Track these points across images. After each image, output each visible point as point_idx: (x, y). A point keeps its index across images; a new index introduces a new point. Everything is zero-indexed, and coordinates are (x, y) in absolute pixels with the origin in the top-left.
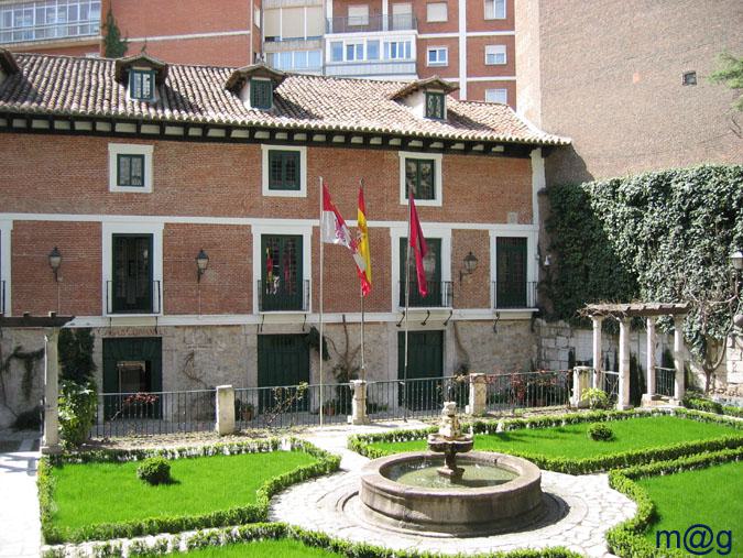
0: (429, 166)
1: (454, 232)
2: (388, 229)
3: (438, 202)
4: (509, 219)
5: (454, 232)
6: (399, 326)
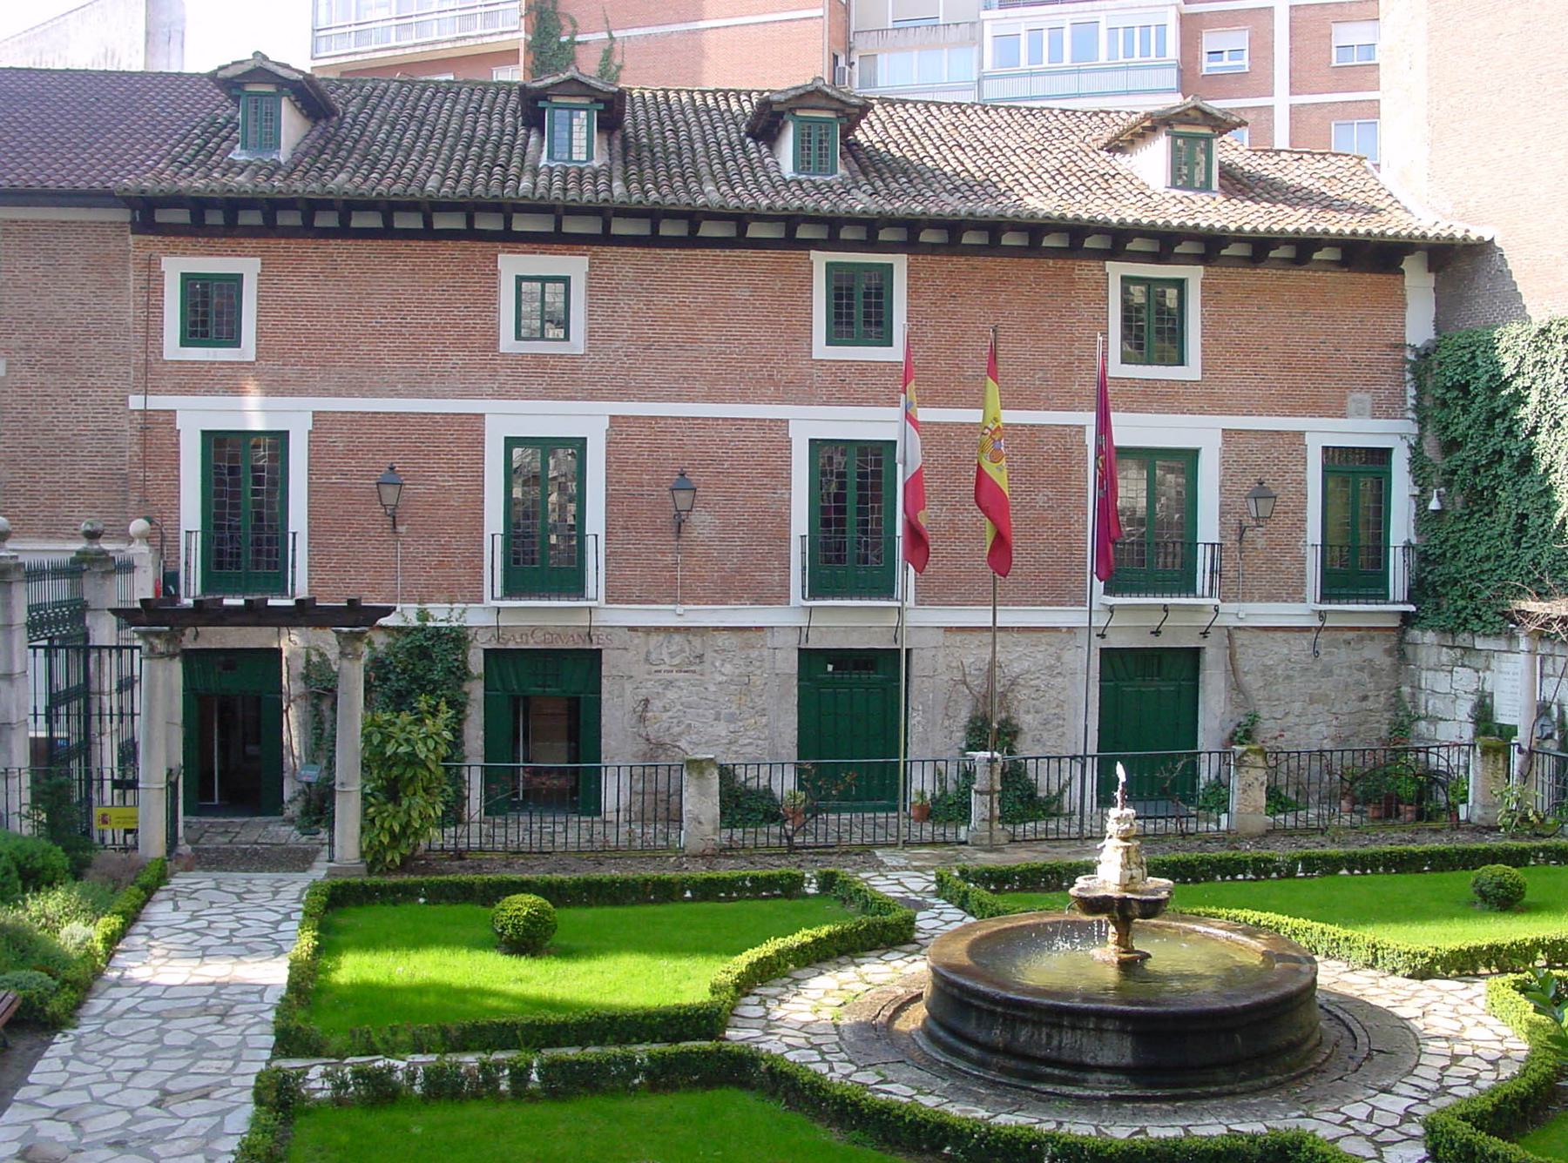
3: (1192, 370)
4: (1351, 407)
6: (1102, 636)
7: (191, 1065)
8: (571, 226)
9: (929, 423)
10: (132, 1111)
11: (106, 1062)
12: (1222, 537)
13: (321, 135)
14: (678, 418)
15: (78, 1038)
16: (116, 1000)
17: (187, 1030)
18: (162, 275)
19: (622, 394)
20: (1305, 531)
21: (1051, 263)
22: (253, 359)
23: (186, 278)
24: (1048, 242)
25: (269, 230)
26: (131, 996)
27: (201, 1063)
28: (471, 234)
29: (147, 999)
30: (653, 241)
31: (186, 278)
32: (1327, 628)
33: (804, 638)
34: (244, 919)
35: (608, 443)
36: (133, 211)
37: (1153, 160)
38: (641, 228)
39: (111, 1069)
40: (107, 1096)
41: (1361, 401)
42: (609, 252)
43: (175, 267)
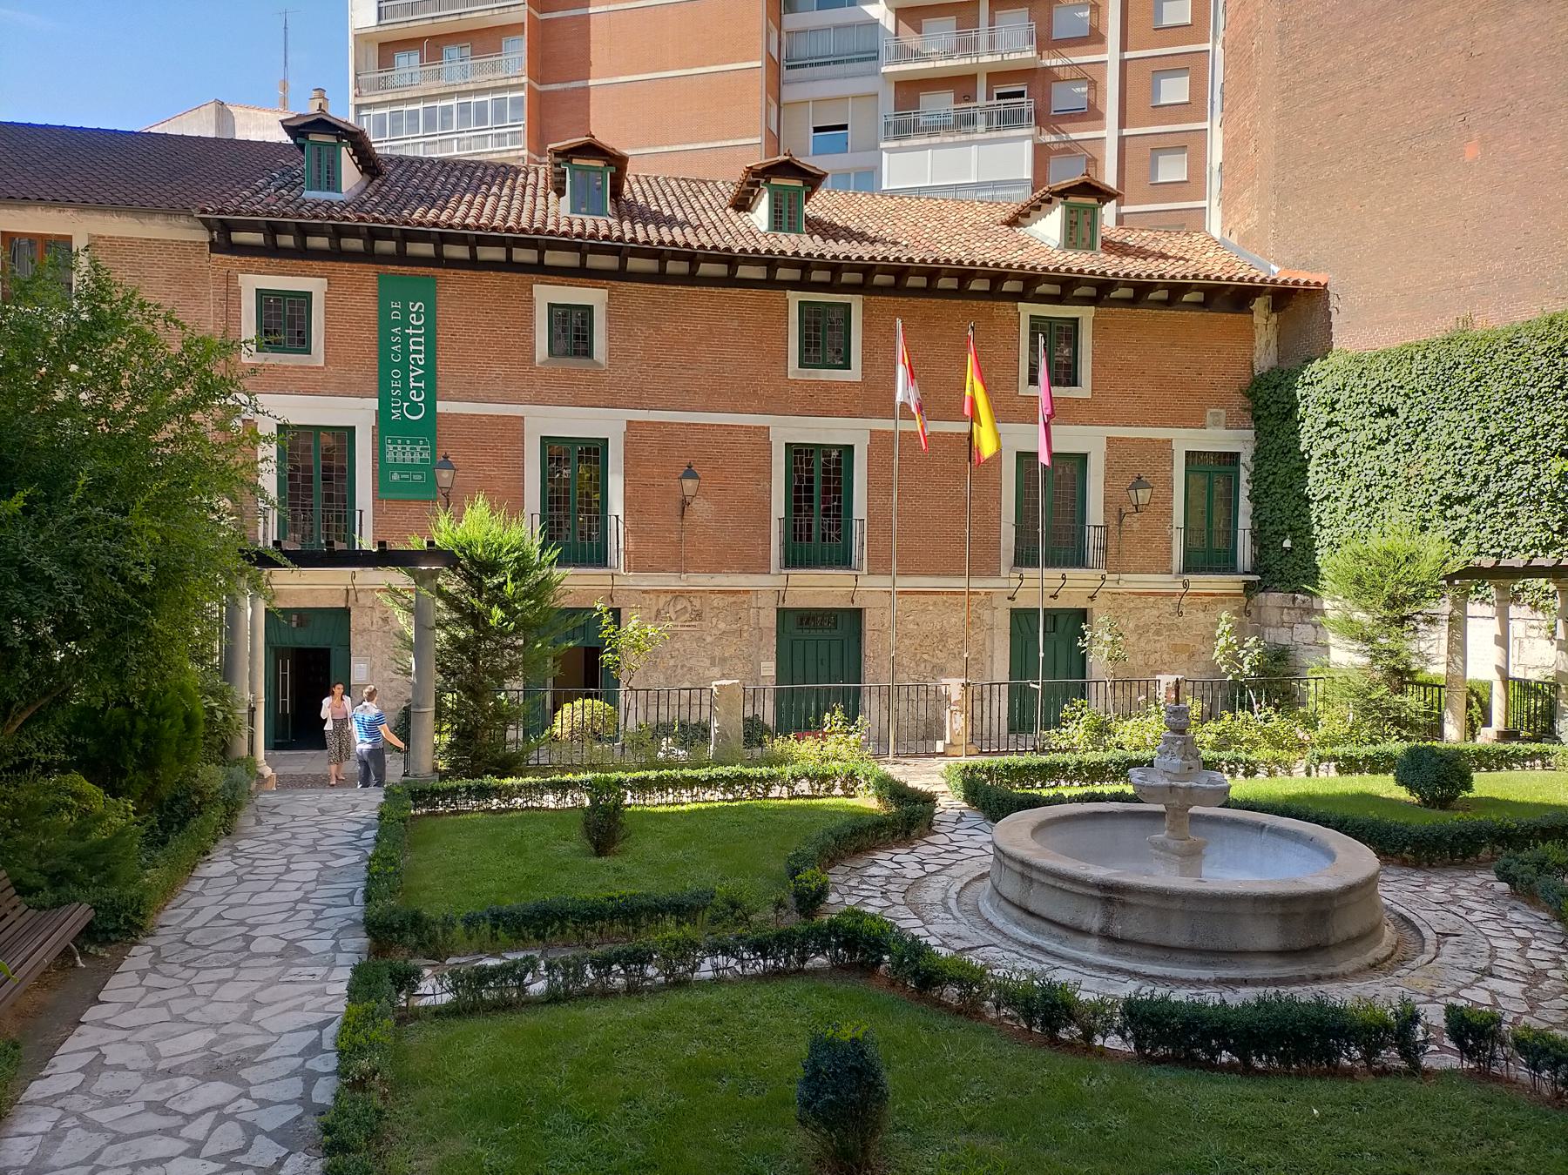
1: (1110, 441)
3: (1083, 391)
4: (1209, 419)
6: (1012, 598)
7: (283, 973)
8: (595, 261)
9: (879, 431)
10: (216, 1026)
11: (188, 973)
12: (1105, 522)
13: (377, 192)
14: (682, 424)
15: (157, 950)
16: (197, 911)
17: (276, 936)
18: (239, 289)
21: (975, 303)
22: (322, 365)
23: (260, 293)
24: (975, 285)
25: (336, 254)
26: (216, 904)
27: (295, 970)
28: (509, 266)
29: (231, 906)
30: (660, 277)
31: (260, 293)
32: (1189, 595)
33: (781, 599)
34: (327, 829)
35: (626, 443)
36: (211, 231)
37: (1049, 227)
38: (650, 265)
39: (195, 980)
40: (189, 1012)
41: (1218, 414)
42: (625, 286)
43: (253, 282)
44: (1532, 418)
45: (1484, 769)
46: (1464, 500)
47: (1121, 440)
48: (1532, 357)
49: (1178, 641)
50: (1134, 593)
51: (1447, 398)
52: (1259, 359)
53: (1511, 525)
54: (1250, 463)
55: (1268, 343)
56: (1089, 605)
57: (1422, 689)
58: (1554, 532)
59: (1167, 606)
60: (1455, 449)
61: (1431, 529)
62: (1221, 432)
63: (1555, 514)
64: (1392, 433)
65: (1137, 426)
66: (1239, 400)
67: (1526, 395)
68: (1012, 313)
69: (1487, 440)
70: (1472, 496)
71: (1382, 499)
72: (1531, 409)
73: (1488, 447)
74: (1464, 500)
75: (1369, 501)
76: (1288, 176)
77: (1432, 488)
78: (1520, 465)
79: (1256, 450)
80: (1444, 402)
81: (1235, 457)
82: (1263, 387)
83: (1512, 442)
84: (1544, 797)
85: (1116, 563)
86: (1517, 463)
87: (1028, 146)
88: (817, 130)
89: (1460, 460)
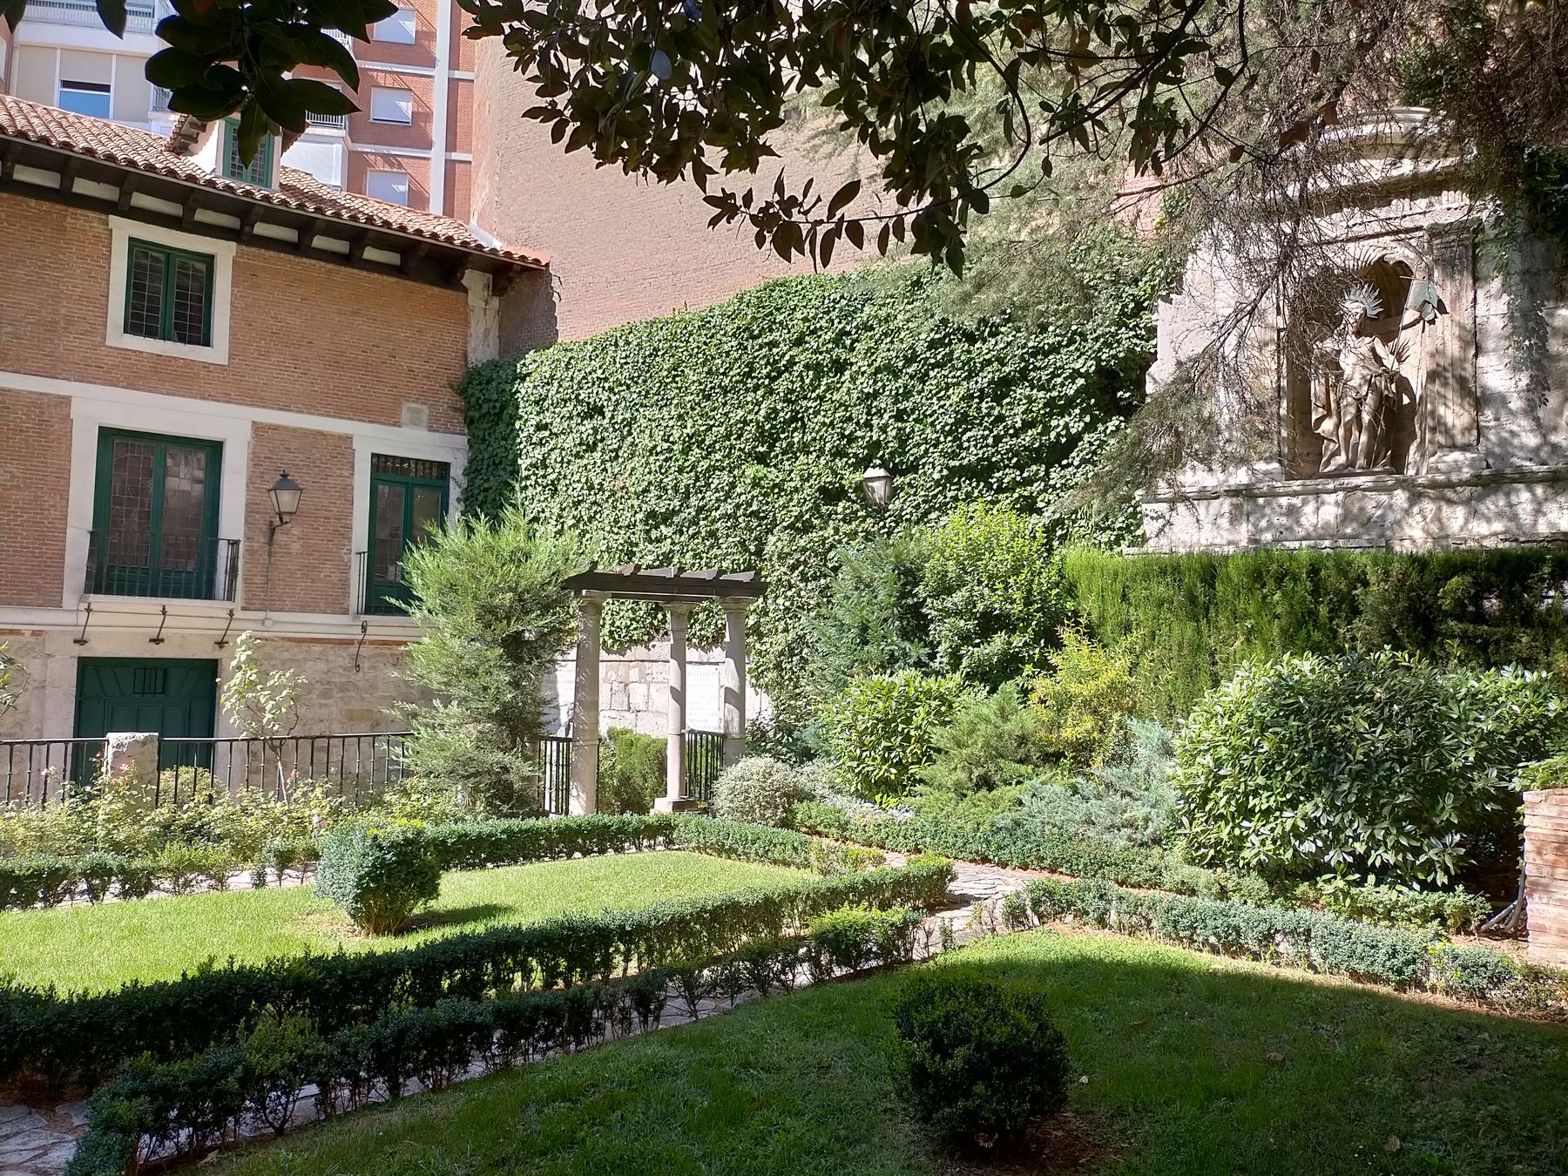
0: (202, 267)
1: (257, 428)
2: (65, 401)
3: (217, 352)
4: (405, 415)
5: (257, 428)
6: (81, 642)
19: (261, 402)
20: (350, 539)
28: (64, 196)
41: (417, 411)
44: (726, 414)
45: (577, 855)
46: (667, 518)
47: (275, 428)
48: (724, 339)
49: (356, 706)
50: (290, 639)
51: (648, 393)
52: (475, 350)
53: (712, 546)
54: (461, 477)
55: (487, 332)
56: (216, 655)
57: (555, 743)
58: (751, 554)
59: (342, 658)
60: (657, 454)
61: (638, 555)
62: (422, 434)
63: (751, 531)
64: (599, 437)
65: (299, 412)
66: (448, 398)
67: (720, 386)
68: (100, 229)
69: (684, 442)
70: (674, 513)
71: (591, 519)
72: (724, 404)
73: (686, 452)
74: (667, 518)
75: (578, 522)
76: (512, 134)
77: (636, 503)
78: (717, 472)
79: (470, 462)
80: (646, 397)
81: (444, 467)
82: (475, 382)
83: (707, 443)
84: (721, 885)
85: (265, 599)
86: (715, 468)
87: (337, 150)
88: (66, 84)
89: (661, 467)
